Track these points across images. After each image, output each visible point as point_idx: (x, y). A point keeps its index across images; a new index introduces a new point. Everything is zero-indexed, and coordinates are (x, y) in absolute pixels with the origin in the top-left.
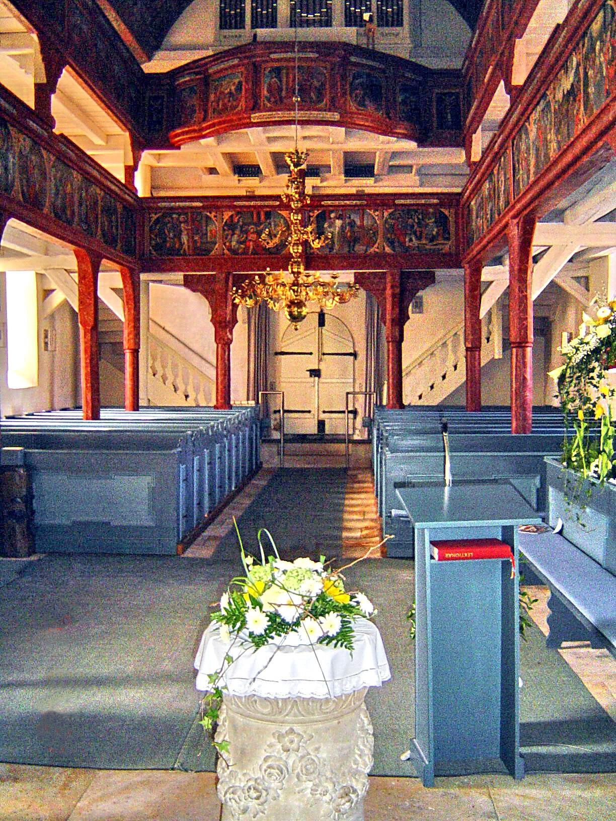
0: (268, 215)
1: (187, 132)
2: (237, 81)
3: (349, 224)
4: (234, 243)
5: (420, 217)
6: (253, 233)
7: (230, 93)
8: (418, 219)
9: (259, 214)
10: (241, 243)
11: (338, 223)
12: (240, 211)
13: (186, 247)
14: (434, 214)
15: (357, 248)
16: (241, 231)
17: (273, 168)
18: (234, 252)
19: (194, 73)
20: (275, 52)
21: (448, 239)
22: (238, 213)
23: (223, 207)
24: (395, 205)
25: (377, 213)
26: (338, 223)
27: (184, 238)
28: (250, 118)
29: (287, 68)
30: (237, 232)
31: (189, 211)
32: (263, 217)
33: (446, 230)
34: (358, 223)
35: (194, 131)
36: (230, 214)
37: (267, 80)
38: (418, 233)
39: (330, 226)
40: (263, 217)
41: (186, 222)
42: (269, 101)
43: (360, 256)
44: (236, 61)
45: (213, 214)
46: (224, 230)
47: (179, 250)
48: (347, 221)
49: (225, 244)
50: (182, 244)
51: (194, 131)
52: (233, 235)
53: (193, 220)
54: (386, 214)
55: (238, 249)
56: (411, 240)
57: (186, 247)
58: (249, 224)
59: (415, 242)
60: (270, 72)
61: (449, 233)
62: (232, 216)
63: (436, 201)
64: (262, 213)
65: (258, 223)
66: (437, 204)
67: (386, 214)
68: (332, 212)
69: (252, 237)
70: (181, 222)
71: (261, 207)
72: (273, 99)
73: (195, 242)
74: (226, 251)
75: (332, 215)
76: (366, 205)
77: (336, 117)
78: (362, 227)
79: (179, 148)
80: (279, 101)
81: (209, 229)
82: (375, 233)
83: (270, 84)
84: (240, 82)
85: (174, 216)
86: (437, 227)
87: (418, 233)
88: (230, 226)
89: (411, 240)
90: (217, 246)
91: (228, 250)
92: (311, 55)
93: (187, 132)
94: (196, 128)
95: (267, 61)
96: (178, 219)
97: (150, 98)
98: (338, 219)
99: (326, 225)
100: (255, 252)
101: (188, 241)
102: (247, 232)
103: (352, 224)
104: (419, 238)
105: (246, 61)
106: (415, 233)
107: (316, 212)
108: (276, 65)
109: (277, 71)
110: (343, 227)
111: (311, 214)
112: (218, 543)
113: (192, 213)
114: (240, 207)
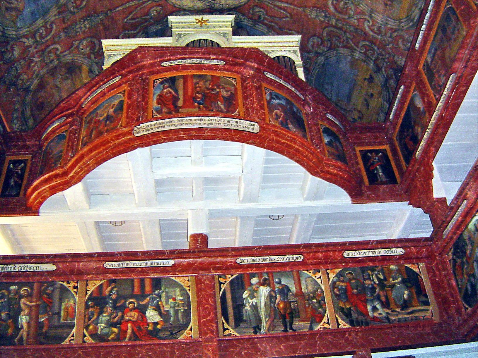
0: (157, 284)
1: (46, 181)
2: (117, 102)
3: (281, 292)
4: (101, 326)
5: (381, 277)
6: (134, 309)
7: (108, 118)
8: (378, 279)
9: (142, 281)
10: (114, 325)
11: (264, 291)
12: (115, 278)
13: (24, 333)
14: (399, 271)
15: (296, 324)
16: (115, 308)
17: (159, 177)
18: (102, 338)
19: (64, 116)
20: (169, 60)
21: (427, 303)
22: (110, 282)
23: (89, 272)
24: (344, 259)
25: (319, 275)
26: (264, 291)
27: (23, 319)
28: (131, 132)
29: (185, 78)
30: (109, 309)
31: (37, 278)
32: (148, 288)
33: (421, 291)
34: (294, 289)
35: (56, 176)
36: (98, 283)
37: (158, 92)
38: (383, 299)
39: (253, 297)
40: (148, 288)
41: (29, 296)
42: (159, 112)
43: (302, 336)
44: (117, 79)
45: (72, 284)
46: (87, 307)
47: (13, 337)
48: (277, 287)
49: (87, 328)
50: (18, 329)
51: (56, 176)
52: (101, 313)
53: (40, 296)
54: (332, 276)
55: (108, 335)
56: (375, 309)
57: (24, 333)
58: (126, 298)
59: (382, 311)
60: (162, 83)
61: (426, 296)
62: (100, 287)
63: (400, 251)
64: (147, 283)
65: (143, 295)
66: (401, 257)
67: (332, 276)
68: (253, 275)
69: (134, 315)
70: (21, 297)
71: (144, 271)
72: (164, 110)
73: (40, 326)
74: (89, 339)
75: (254, 281)
76: (303, 263)
77: (255, 128)
78: (300, 294)
79: (36, 213)
80: (170, 107)
81: (63, 306)
82: (321, 304)
83: (161, 96)
84: (122, 102)
85: (12, 288)
86: (408, 288)
87: (383, 299)
88: (98, 301)
89: (375, 309)
90: (74, 330)
91: (92, 336)
92: (216, 62)
93: (46, 181)
94: (59, 171)
95: (158, 72)
96: (17, 292)
97: (11, 162)
98: (263, 284)
99: (245, 295)
100: (135, 336)
101: (28, 323)
102: (123, 309)
103: (285, 291)
104: (386, 305)
105: (130, 76)
106: (378, 298)
107: (230, 278)
108: (169, 75)
109: (172, 81)
110: (271, 297)
111: (222, 280)
112: (436, 319)
113: (41, 283)
114: (115, 271)
